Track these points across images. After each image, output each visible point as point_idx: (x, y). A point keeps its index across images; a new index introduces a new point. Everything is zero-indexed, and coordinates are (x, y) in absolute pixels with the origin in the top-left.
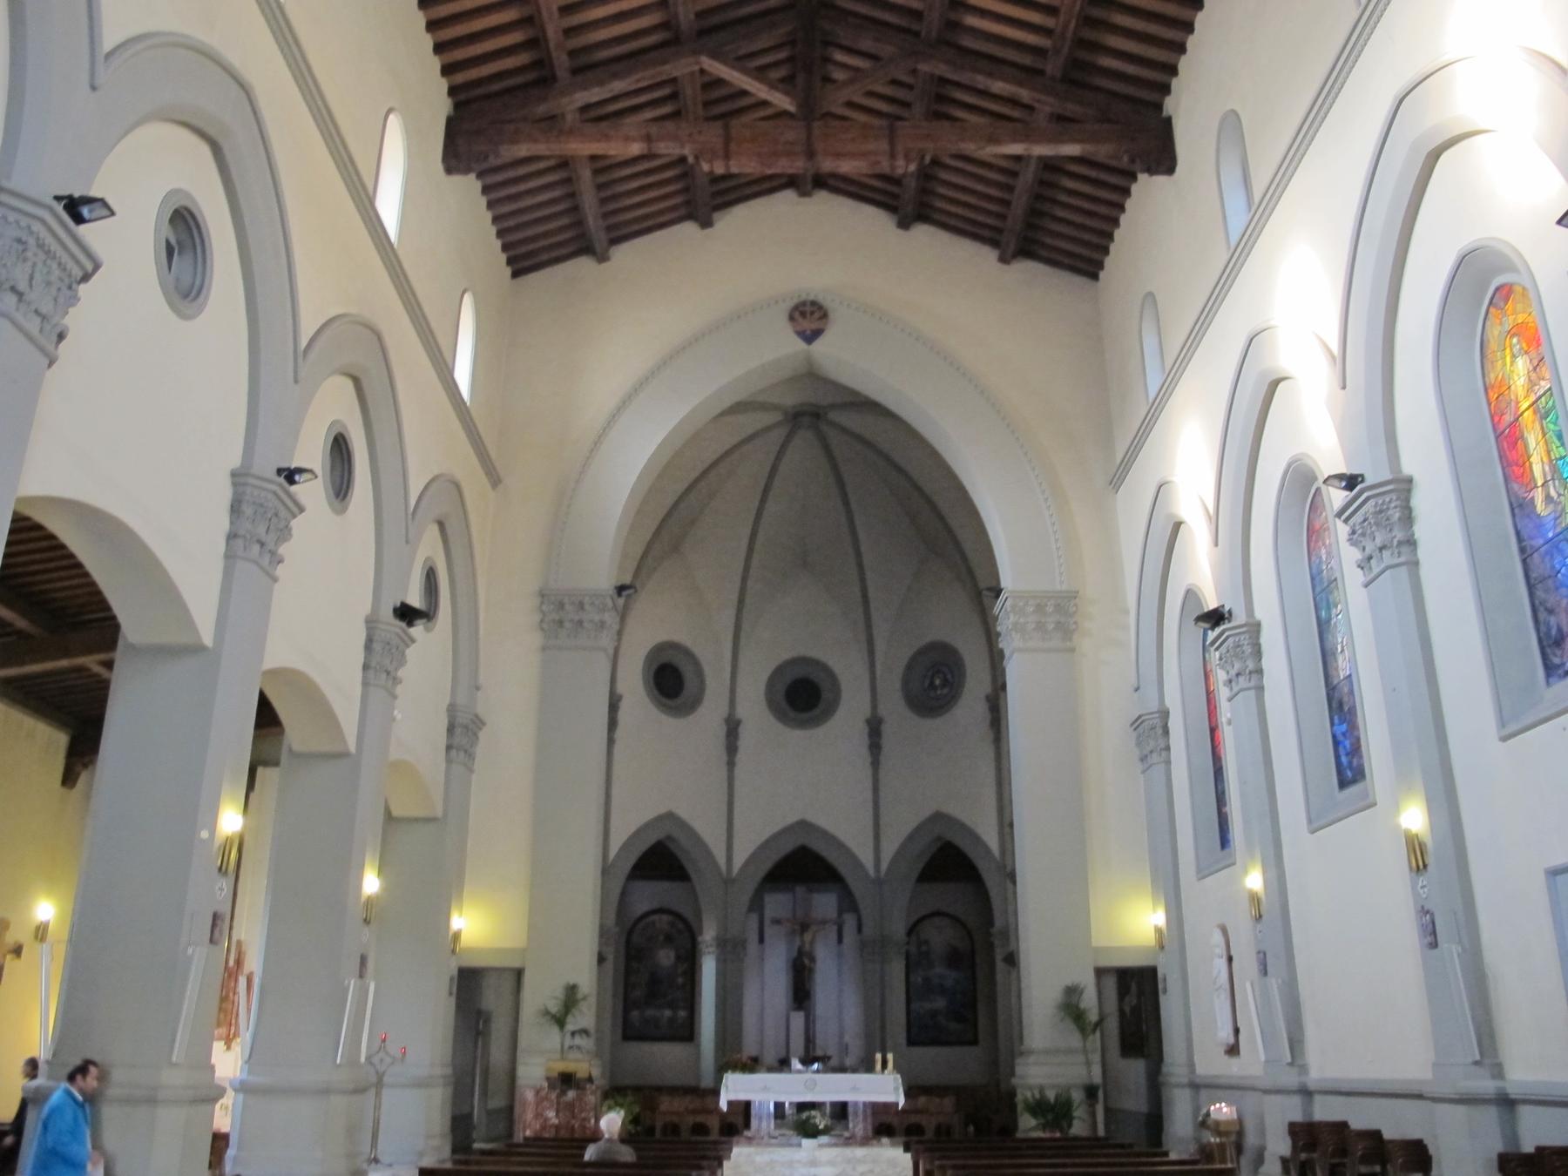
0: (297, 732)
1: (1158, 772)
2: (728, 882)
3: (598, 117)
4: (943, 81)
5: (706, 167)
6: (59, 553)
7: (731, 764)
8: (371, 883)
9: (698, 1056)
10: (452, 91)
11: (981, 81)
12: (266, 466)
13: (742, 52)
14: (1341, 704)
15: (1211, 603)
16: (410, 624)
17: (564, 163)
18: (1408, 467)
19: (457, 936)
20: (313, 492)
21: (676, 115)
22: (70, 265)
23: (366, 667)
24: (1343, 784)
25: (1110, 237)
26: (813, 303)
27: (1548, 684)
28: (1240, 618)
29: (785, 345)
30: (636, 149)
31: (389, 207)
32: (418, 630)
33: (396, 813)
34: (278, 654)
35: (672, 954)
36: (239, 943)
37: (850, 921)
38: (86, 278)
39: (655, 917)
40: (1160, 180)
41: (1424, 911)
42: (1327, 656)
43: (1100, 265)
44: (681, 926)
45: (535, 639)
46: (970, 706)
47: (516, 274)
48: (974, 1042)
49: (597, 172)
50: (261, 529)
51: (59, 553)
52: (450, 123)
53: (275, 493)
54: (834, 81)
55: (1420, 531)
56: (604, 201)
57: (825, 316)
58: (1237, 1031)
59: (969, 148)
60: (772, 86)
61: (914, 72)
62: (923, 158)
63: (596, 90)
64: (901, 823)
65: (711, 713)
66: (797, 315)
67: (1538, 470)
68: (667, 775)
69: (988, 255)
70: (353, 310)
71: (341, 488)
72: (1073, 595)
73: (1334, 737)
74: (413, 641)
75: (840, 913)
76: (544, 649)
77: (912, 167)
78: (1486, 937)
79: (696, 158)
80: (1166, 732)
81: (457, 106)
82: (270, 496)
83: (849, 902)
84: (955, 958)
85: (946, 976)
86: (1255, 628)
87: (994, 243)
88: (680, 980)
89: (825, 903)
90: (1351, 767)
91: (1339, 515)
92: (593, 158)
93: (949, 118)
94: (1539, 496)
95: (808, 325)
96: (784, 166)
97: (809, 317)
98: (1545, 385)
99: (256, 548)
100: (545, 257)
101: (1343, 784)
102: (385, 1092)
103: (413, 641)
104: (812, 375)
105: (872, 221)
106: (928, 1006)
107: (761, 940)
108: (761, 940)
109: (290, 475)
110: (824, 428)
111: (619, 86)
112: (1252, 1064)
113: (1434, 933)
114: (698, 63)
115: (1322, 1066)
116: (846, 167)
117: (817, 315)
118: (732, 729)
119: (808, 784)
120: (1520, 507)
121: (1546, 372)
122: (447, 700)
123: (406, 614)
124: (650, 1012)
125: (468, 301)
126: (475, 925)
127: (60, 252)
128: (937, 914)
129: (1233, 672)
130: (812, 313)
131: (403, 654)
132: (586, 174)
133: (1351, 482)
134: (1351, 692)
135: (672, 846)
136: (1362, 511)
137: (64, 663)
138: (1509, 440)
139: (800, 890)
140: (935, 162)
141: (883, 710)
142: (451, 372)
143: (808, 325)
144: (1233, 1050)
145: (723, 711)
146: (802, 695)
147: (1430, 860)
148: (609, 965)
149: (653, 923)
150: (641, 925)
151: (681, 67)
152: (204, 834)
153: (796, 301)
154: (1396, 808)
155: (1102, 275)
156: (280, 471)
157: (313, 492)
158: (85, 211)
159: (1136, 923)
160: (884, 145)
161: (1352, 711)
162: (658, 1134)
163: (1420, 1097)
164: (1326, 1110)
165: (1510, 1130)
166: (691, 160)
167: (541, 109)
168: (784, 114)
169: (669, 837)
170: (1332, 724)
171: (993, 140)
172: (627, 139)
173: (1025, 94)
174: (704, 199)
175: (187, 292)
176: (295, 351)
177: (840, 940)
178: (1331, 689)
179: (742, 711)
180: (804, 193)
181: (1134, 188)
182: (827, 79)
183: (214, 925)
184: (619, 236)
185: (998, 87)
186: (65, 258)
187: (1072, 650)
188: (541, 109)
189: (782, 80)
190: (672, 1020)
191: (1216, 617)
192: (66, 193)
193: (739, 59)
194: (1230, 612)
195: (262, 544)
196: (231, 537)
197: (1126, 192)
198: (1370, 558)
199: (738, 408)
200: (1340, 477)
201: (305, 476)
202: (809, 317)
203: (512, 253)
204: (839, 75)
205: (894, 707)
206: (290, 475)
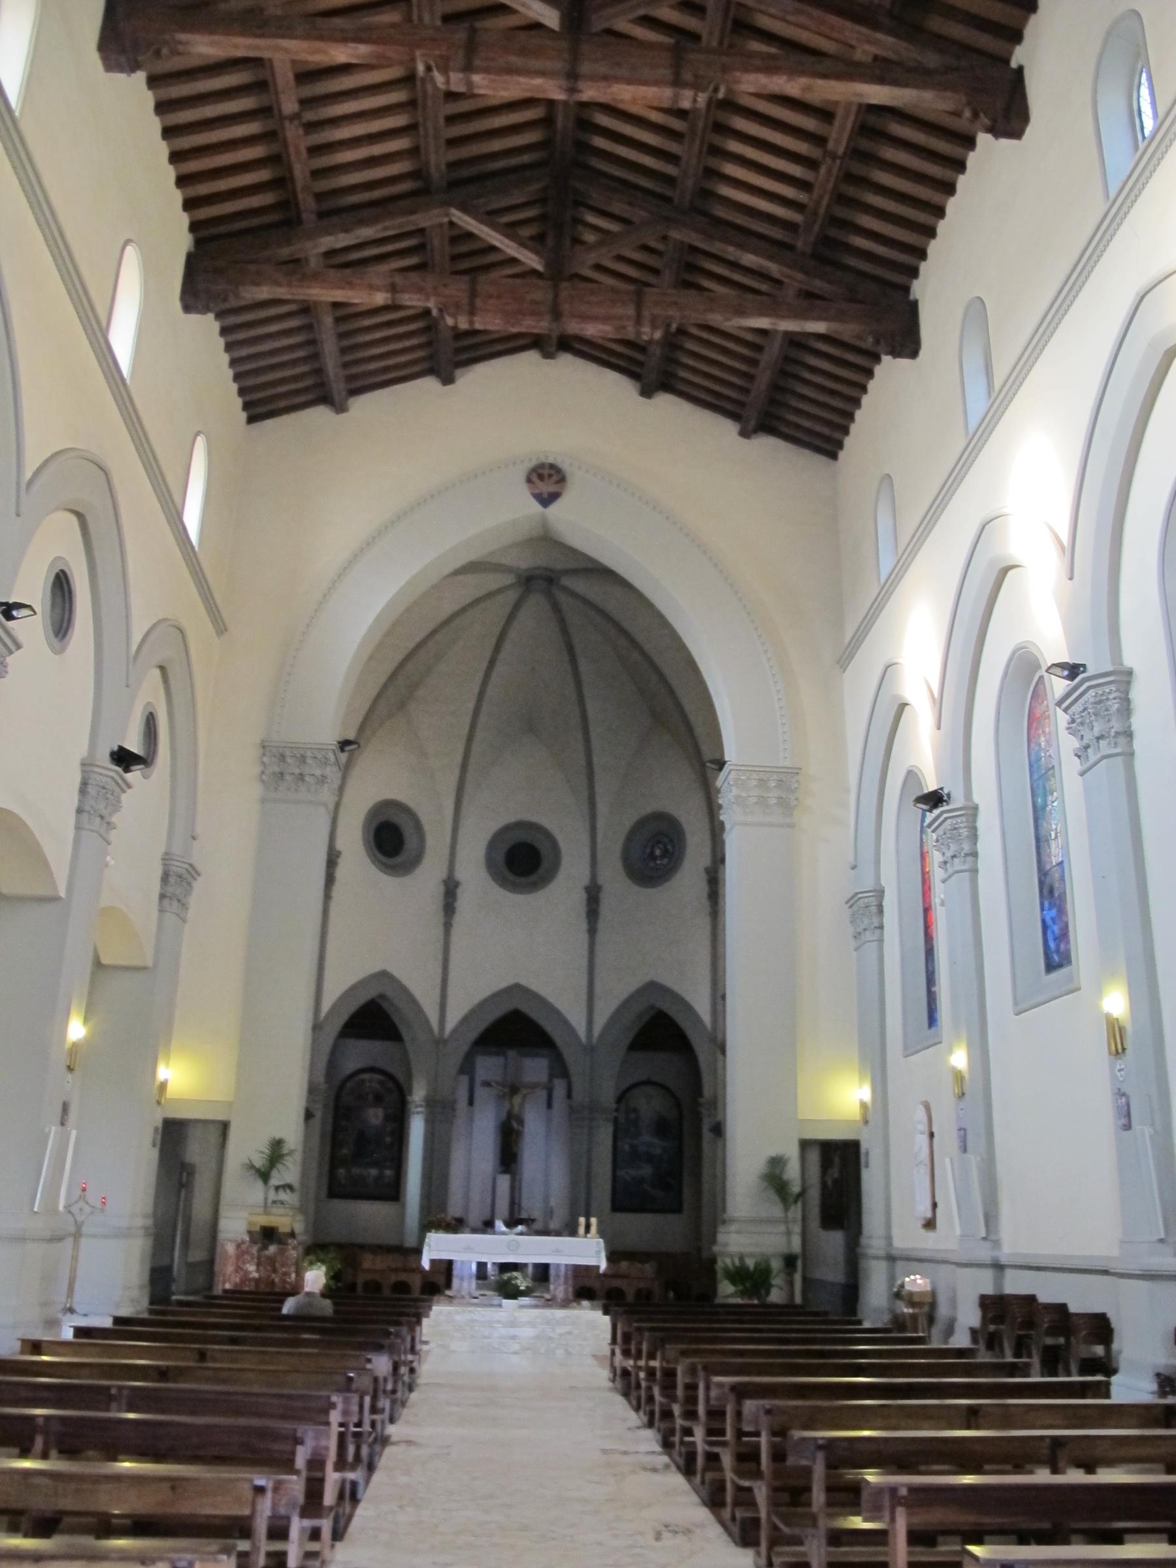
2: (440, 1042)
3: (343, 263)
4: (694, 249)
7: (448, 926)
9: (402, 1215)
10: (194, 227)
11: (731, 252)
13: (495, 205)
15: (931, 786)
16: (127, 770)
17: (306, 309)
19: (163, 1086)
20: (30, 629)
21: (420, 267)
24: (1050, 967)
25: (851, 417)
28: (958, 801)
29: (522, 507)
30: (380, 298)
32: (135, 776)
39: (366, 1076)
40: (904, 362)
41: (1121, 1094)
42: (1041, 842)
44: (390, 1085)
47: (251, 420)
48: (678, 1210)
49: (338, 320)
52: (190, 258)
54: (582, 243)
55: (1137, 722)
56: (344, 351)
57: (562, 480)
59: (716, 319)
60: (522, 244)
61: (665, 238)
62: (669, 326)
63: (342, 236)
64: (615, 991)
66: (535, 478)
68: (384, 933)
69: (729, 428)
71: (61, 626)
72: (796, 772)
73: (1044, 921)
74: (129, 787)
76: (263, 801)
77: (658, 335)
79: (441, 310)
80: (880, 910)
81: (198, 242)
83: (560, 1069)
84: (662, 1128)
86: (972, 811)
88: (388, 1139)
89: (535, 1068)
90: (1058, 951)
91: (1059, 704)
92: (336, 305)
93: (701, 289)
95: (546, 488)
97: (547, 480)
100: (283, 404)
101: (1050, 967)
104: (546, 539)
105: (615, 388)
106: (633, 1172)
107: (471, 1103)
108: (471, 1103)
109: (9, 610)
111: (367, 232)
112: (948, 1238)
114: (447, 215)
116: (591, 330)
117: (555, 478)
118: (451, 890)
119: (520, 948)
123: (124, 759)
124: (356, 1171)
125: (200, 444)
128: (648, 1082)
129: (949, 854)
130: (550, 476)
131: (119, 801)
132: (328, 320)
133: (1073, 671)
134: (1062, 879)
135: (385, 1005)
136: (1081, 701)
139: (512, 1054)
140: (682, 331)
143: (546, 488)
148: (317, 1121)
149: (363, 1081)
150: (349, 1085)
151: (429, 219)
154: (1099, 993)
155: (842, 454)
157: (30, 629)
160: (630, 311)
161: (1062, 897)
163: (1106, 1272)
164: (1016, 1285)
166: (435, 312)
167: (285, 252)
168: (534, 272)
169: (382, 996)
170: (1042, 909)
171: (741, 312)
172: (372, 288)
173: (774, 268)
174: (447, 354)
176: (18, 484)
177: (549, 1105)
178: (1043, 873)
179: (461, 874)
180: (548, 355)
182: (577, 241)
185: (749, 259)
188: (285, 252)
189: (532, 238)
190: (380, 1177)
193: (490, 213)
194: (949, 795)
198: (1087, 747)
202: (547, 480)
203: (248, 398)
204: (590, 237)
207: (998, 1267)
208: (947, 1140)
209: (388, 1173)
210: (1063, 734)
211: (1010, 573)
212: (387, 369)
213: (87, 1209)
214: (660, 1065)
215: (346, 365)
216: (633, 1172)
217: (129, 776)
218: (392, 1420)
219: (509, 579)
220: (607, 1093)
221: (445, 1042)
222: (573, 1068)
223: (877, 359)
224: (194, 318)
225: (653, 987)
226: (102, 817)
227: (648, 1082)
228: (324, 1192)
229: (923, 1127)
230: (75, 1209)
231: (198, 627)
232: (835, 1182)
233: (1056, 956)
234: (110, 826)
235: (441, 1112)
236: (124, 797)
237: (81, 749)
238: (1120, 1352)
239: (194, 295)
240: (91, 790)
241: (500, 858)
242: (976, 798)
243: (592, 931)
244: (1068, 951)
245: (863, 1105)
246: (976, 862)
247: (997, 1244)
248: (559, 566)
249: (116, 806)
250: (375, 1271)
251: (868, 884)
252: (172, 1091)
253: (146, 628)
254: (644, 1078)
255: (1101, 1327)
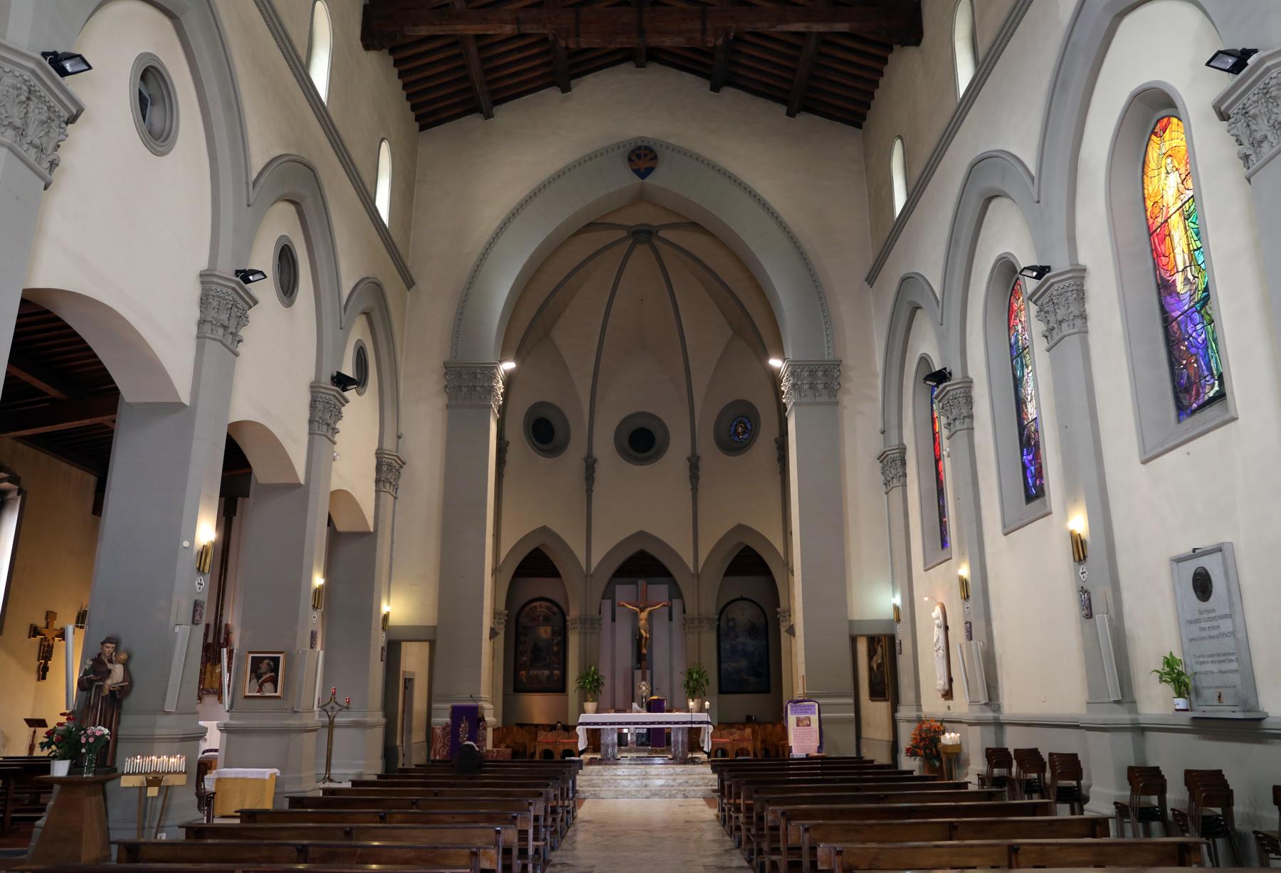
0: (262, 472)
1: (896, 493)
2: (587, 576)
5: (563, 43)
6: (65, 331)
8: (318, 580)
9: (566, 704)
12: (227, 268)
14: (1029, 438)
16: (345, 390)
17: (457, 41)
18: (1084, 259)
19: (386, 617)
20: (265, 290)
22: (58, 107)
23: (311, 422)
24: (1029, 498)
25: (871, 95)
26: (646, 148)
27: (1179, 421)
28: (957, 375)
29: (626, 179)
30: (509, 29)
31: (320, 74)
32: (351, 394)
33: (341, 527)
34: (241, 411)
35: (549, 629)
36: (227, 625)
37: (677, 604)
38: (72, 119)
39: (537, 604)
41: (1083, 591)
42: (1020, 403)
43: (863, 117)
44: (555, 609)
45: (441, 401)
46: (763, 446)
47: (422, 129)
48: (768, 691)
49: (480, 49)
50: (224, 316)
51: (65, 331)
53: (234, 289)
55: (1091, 307)
57: (655, 158)
58: (950, 680)
59: (763, 27)
62: (727, 35)
64: (714, 532)
65: (573, 456)
66: (634, 158)
67: (1181, 259)
70: (293, 151)
71: (288, 287)
72: (838, 364)
73: (1023, 464)
75: (670, 599)
76: (448, 407)
77: (720, 42)
78: (1126, 609)
80: (904, 463)
82: (230, 291)
83: (676, 593)
84: (753, 631)
85: (750, 644)
86: (968, 383)
87: (782, 101)
88: (555, 649)
89: (659, 591)
91: (1030, 298)
92: (478, 37)
94: (1179, 278)
95: (643, 165)
96: (620, 42)
98: (1190, 193)
99: (221, 331)
100: (444, 115)
101: (1029, 498)
102: (336, 732)
103: (347, 402)
105: (693, 85)
106: (733, 665)
107: (613, 620)
108: (613, 620)
109: (245, 276)
110: (657, 243)
112: (961, 706)
113: (1090, 607)
115: (1014, 703)
116: (668, 42)
119: (642, 505)
120: (1165, 287)
121: (1189, 184)
122: (376, 446)
123: (341, 381)
125: (385, 147)
126: (397, 607)
127: (49, 97)
128: (742, 599)
129: (951, 417)
131: (340, 412)
132: (473, 49)
133: (1041, 271)
134: (1036, 431)
136: (1048, 294)
137: (87, 422)
138: (1156, 236)
139: (641, 582)
141: (699, 451)
142: (373, 201)
143: (643, 165)
144: (948, 694)
145: (584, 453)
146: (642, 441)
147: (1089, 552)
150: (527, 609)
152: (186, 544)
153: (633, 146)
154: (1065, 517)
155: (865, 124)
156: (237, 273)
157: (265, 290)
158: (68, 66)
159: (881, 602)
161: (1037, 445)
162: (537, 758)
163: (1077, 727)
164: (1014, 741)
165: (1139, 749)
170: (1022, 455)
175: (158, 136)
177: (671, 619)
179: (597, 453)
181: (890, 57)
183: (195, 611)
184: (502, 96)
186: (53, 102)
187: (837, 404)
190: (548, 677)
191: (941, 377)
192: (51, 50)
194: (950, 374)
195: (225, 328)
196: (201, 323)
197: (885, 61)
198: (1053, 329)
199: (591, 226)
200: (1031, 268)
201: (258, 277)
202: (643, 158)
203: (419, 112)
205: (605, 447)
206: (245, 276)
207: (999, 725)
208: (957, 633)
209: (556, 672)
210: (1034, 321)
211: (994, 203)
212: (520, 84)
213: (337, 708)
214: (747, 585)
215: (489, 83)
216: (733, 665)
217: (346, 394)
218: (553, 849)
219: (622, 234)
220: (709, 606)
221: (591, 576)
222: (684, 593)
223: (891, 49)
224: (373, 55)
225: (740, 528)
226: (328, 425)
227: (742, 599)
228: (511, 689)
229: (940, 621)
230: (328, 708)
231: (392, 285)
232: (879, 666)
233: (1034, 490)
234: (335, 431)
235: (590, 624)
236: (343, 409)
237: (309, 375)
238: (1089, 786)
239: (370, 39)
240: (320, 406)
241: (626, 444)
242: (971, 374)
243: (695, 490)
244: (1042, 485)
245: (896, 609)
246: (972, 422)
247: (998, 709)
248: (656, 223)
249: (339, 416)
250: (548, 743)
251: (894, 442)
252: (393, 621)
253: (352, 286)
254: (738, 596)
255: (1070, 765)
